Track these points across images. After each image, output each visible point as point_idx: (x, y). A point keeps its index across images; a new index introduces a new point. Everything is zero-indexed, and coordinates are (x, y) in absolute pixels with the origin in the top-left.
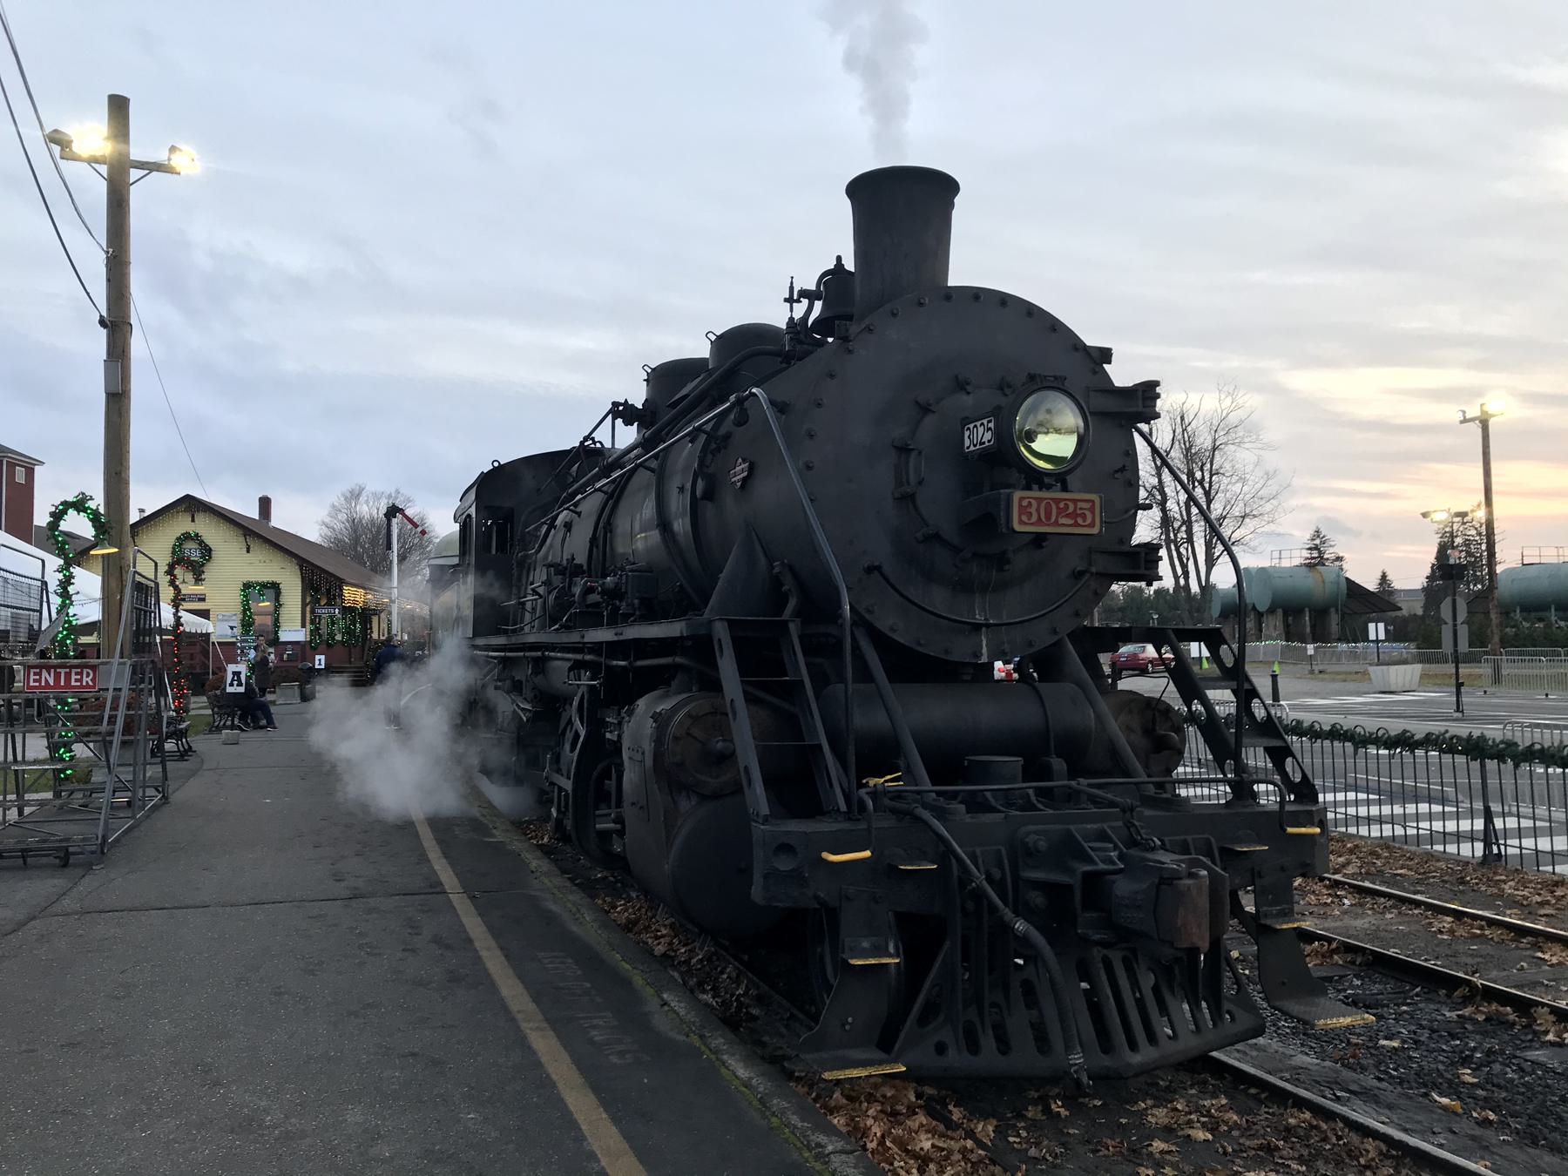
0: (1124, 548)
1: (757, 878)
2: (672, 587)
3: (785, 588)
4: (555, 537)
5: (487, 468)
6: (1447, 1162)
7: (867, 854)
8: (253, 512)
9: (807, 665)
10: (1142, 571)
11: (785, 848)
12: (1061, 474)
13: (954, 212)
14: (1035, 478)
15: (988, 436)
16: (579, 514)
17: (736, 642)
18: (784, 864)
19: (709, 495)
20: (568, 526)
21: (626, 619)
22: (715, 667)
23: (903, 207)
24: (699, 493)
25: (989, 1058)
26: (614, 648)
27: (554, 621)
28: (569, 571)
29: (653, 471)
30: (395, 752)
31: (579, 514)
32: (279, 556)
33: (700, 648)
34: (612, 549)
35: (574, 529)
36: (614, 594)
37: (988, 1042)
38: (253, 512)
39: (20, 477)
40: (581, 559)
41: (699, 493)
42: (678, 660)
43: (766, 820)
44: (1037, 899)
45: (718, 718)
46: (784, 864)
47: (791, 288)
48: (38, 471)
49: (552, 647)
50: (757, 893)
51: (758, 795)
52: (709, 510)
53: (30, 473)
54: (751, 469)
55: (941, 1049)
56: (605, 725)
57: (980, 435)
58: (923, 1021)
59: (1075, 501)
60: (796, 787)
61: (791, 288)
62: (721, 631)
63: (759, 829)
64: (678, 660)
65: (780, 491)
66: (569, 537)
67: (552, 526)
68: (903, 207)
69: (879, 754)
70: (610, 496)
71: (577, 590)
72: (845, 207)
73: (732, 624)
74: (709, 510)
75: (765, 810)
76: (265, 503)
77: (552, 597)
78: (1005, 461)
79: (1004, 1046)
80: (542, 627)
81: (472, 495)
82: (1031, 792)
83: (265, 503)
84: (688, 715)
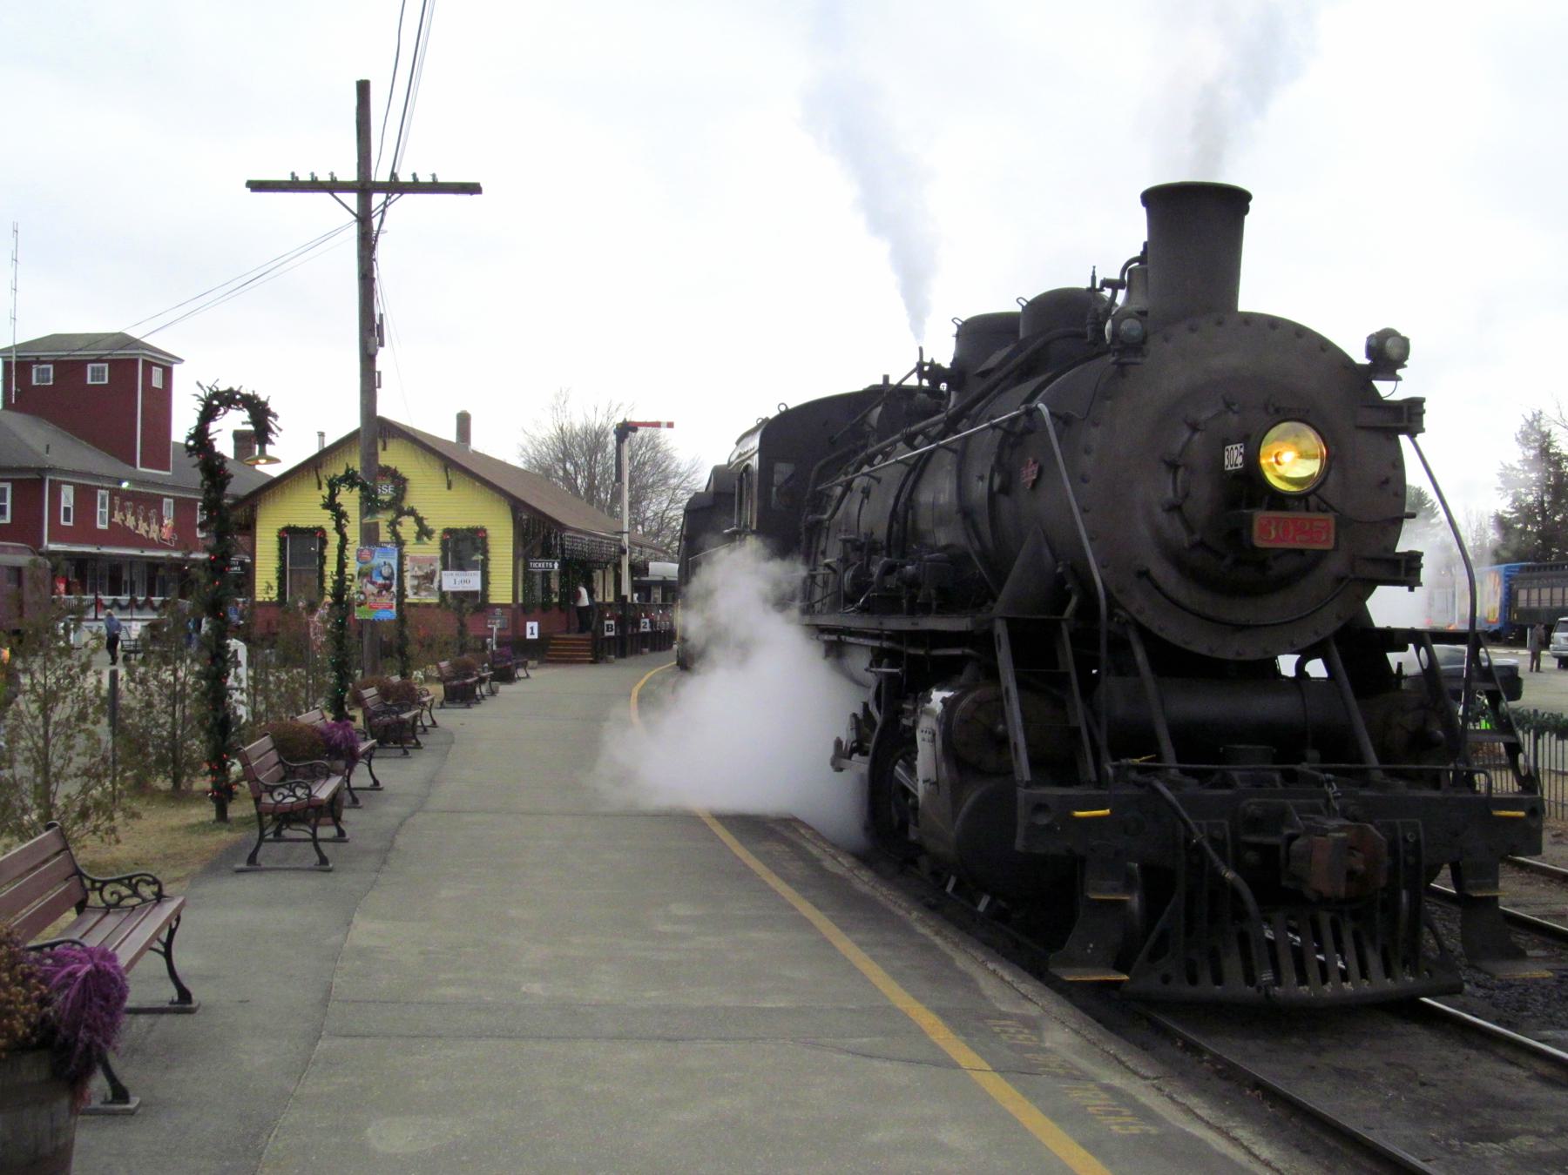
0: (1389, 556)
1: (1020, 831)
2: (960, 585)
3: (1068, 586)
4: (852, 504)
5: (772, 413)
6: (1475, 1024)
7: (1107, 811)
8: (449, 433)
9: (1075, 655)
10: (1402, 577)
11: (1040, 807)
12: (1309, 497)
13: (1247, 218)
14: (1278, 500)
15: (1240, 460)
16: (879, 480)
17: (1013, 637)
18: (1043, 820)
19: (1006, 489)
20: (866, 492)
21: (926, 609)
22: (995, 658)
23: (1197, 221)
24: (996, 487)
25: (1207, 988)
26: (915, 637)
27: (850, 600)
28: (862, 548)
29: (955, 451)
30: (754, 708)
31: (879, 480)
32: (488, 493)
33: (983, 641)
34: (914, 522)
35: (872, 496)
36: (913, 583)
37: (1206, 977)
38: (449, 433)
39: (157, 382)
40: (881, 533)
41: (996, 487)
42: (967, 651)
43: (1028, 785)
44: (1251, 857)
45: (997, 705)
46: (1043, 820)
47: (1094, 278)
48: (176, 368)
49: (852, 633)
50: (1019, 844)
51: (1023, 767)
52: (1004, 503)
53: (167, 374)
54: (1040, 472)
55: (1166, 979)
56: (902, 712)
57: (1234, 457)
58: (1153, 956)
59: (1312, 521)
60: (1056, 764)
61: (1094, 278)
62: (1001, 629)
63: (1022, 793)
64: (967, 651)
65: (1066, 501)
66: (863, 506)
67: (848, 487)
68: (1197, 221)
69: (1133, 739)
70: (912, 468)
71: (876, 570)
72: (1142, 213)
73: (1011, 622)
74: (1004, 503)
75: (1027, 777)
76: (464, 421)
77: (848, 575)
78: (1251, 486)
79: (1218, 980)
80: (834, 607)
81: (755, 442)
82: (1277, 777)
83: (464, 421)
84: (974, 700)
